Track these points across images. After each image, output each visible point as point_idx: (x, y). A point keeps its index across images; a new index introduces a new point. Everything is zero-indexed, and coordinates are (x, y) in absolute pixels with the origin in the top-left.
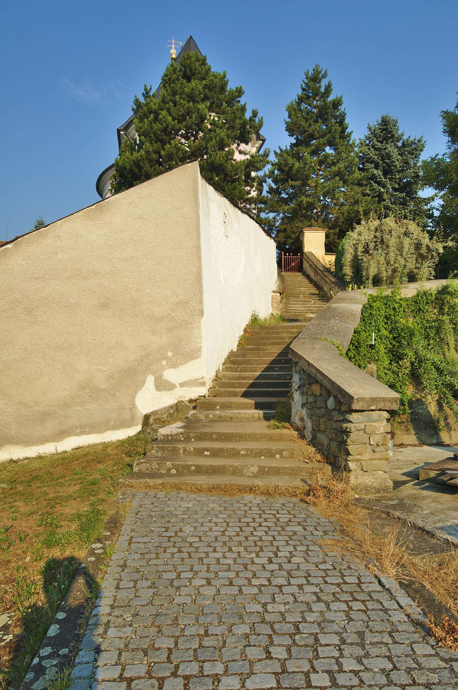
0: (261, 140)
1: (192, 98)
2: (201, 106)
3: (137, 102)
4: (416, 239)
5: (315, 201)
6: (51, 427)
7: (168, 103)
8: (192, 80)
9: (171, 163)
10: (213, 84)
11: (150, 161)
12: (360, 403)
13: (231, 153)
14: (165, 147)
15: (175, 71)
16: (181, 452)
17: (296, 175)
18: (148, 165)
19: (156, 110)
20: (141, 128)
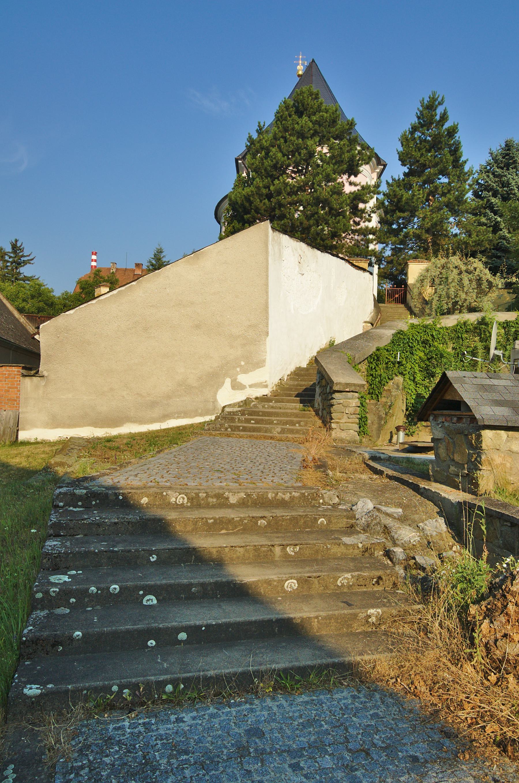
0: (381, 165)
1: (302, 135)
2: (310, 142)
3: (250, 139)
4: (478, 275)
5: (422, 233)
6: (157, 412)
7: (279, 140)
8: (304, 116)
9: (280, 198)
10: (323, 119)
11: (260, 195)
12: (338, 386)
13: (342, 185)
14: (275, 182)
15: (287, 108)
16: (237, 420)
17: (404, 206)
18: (258, 200)
19: (267, 147)
20: (253, 164)
